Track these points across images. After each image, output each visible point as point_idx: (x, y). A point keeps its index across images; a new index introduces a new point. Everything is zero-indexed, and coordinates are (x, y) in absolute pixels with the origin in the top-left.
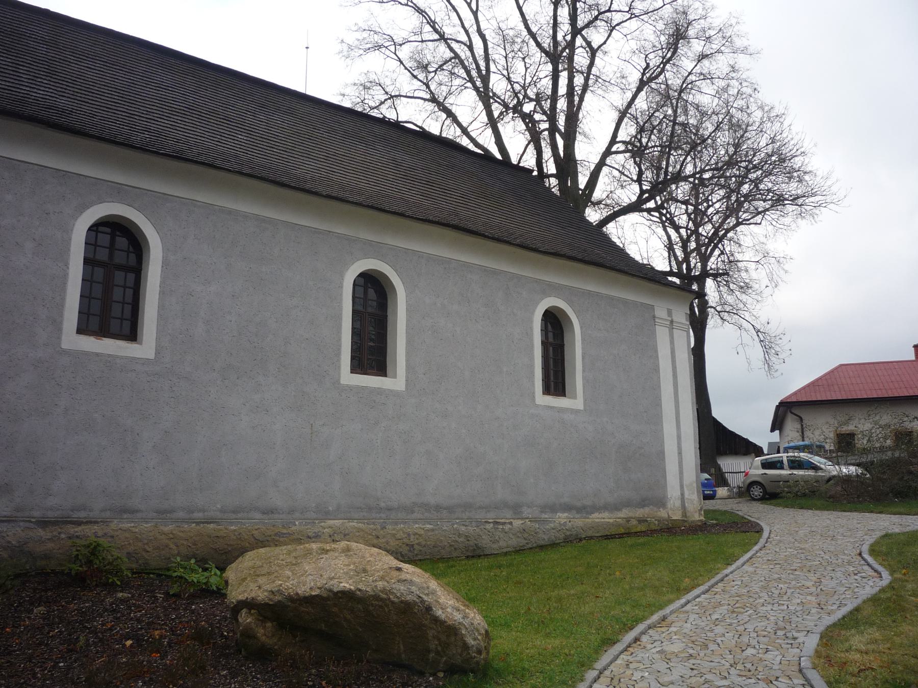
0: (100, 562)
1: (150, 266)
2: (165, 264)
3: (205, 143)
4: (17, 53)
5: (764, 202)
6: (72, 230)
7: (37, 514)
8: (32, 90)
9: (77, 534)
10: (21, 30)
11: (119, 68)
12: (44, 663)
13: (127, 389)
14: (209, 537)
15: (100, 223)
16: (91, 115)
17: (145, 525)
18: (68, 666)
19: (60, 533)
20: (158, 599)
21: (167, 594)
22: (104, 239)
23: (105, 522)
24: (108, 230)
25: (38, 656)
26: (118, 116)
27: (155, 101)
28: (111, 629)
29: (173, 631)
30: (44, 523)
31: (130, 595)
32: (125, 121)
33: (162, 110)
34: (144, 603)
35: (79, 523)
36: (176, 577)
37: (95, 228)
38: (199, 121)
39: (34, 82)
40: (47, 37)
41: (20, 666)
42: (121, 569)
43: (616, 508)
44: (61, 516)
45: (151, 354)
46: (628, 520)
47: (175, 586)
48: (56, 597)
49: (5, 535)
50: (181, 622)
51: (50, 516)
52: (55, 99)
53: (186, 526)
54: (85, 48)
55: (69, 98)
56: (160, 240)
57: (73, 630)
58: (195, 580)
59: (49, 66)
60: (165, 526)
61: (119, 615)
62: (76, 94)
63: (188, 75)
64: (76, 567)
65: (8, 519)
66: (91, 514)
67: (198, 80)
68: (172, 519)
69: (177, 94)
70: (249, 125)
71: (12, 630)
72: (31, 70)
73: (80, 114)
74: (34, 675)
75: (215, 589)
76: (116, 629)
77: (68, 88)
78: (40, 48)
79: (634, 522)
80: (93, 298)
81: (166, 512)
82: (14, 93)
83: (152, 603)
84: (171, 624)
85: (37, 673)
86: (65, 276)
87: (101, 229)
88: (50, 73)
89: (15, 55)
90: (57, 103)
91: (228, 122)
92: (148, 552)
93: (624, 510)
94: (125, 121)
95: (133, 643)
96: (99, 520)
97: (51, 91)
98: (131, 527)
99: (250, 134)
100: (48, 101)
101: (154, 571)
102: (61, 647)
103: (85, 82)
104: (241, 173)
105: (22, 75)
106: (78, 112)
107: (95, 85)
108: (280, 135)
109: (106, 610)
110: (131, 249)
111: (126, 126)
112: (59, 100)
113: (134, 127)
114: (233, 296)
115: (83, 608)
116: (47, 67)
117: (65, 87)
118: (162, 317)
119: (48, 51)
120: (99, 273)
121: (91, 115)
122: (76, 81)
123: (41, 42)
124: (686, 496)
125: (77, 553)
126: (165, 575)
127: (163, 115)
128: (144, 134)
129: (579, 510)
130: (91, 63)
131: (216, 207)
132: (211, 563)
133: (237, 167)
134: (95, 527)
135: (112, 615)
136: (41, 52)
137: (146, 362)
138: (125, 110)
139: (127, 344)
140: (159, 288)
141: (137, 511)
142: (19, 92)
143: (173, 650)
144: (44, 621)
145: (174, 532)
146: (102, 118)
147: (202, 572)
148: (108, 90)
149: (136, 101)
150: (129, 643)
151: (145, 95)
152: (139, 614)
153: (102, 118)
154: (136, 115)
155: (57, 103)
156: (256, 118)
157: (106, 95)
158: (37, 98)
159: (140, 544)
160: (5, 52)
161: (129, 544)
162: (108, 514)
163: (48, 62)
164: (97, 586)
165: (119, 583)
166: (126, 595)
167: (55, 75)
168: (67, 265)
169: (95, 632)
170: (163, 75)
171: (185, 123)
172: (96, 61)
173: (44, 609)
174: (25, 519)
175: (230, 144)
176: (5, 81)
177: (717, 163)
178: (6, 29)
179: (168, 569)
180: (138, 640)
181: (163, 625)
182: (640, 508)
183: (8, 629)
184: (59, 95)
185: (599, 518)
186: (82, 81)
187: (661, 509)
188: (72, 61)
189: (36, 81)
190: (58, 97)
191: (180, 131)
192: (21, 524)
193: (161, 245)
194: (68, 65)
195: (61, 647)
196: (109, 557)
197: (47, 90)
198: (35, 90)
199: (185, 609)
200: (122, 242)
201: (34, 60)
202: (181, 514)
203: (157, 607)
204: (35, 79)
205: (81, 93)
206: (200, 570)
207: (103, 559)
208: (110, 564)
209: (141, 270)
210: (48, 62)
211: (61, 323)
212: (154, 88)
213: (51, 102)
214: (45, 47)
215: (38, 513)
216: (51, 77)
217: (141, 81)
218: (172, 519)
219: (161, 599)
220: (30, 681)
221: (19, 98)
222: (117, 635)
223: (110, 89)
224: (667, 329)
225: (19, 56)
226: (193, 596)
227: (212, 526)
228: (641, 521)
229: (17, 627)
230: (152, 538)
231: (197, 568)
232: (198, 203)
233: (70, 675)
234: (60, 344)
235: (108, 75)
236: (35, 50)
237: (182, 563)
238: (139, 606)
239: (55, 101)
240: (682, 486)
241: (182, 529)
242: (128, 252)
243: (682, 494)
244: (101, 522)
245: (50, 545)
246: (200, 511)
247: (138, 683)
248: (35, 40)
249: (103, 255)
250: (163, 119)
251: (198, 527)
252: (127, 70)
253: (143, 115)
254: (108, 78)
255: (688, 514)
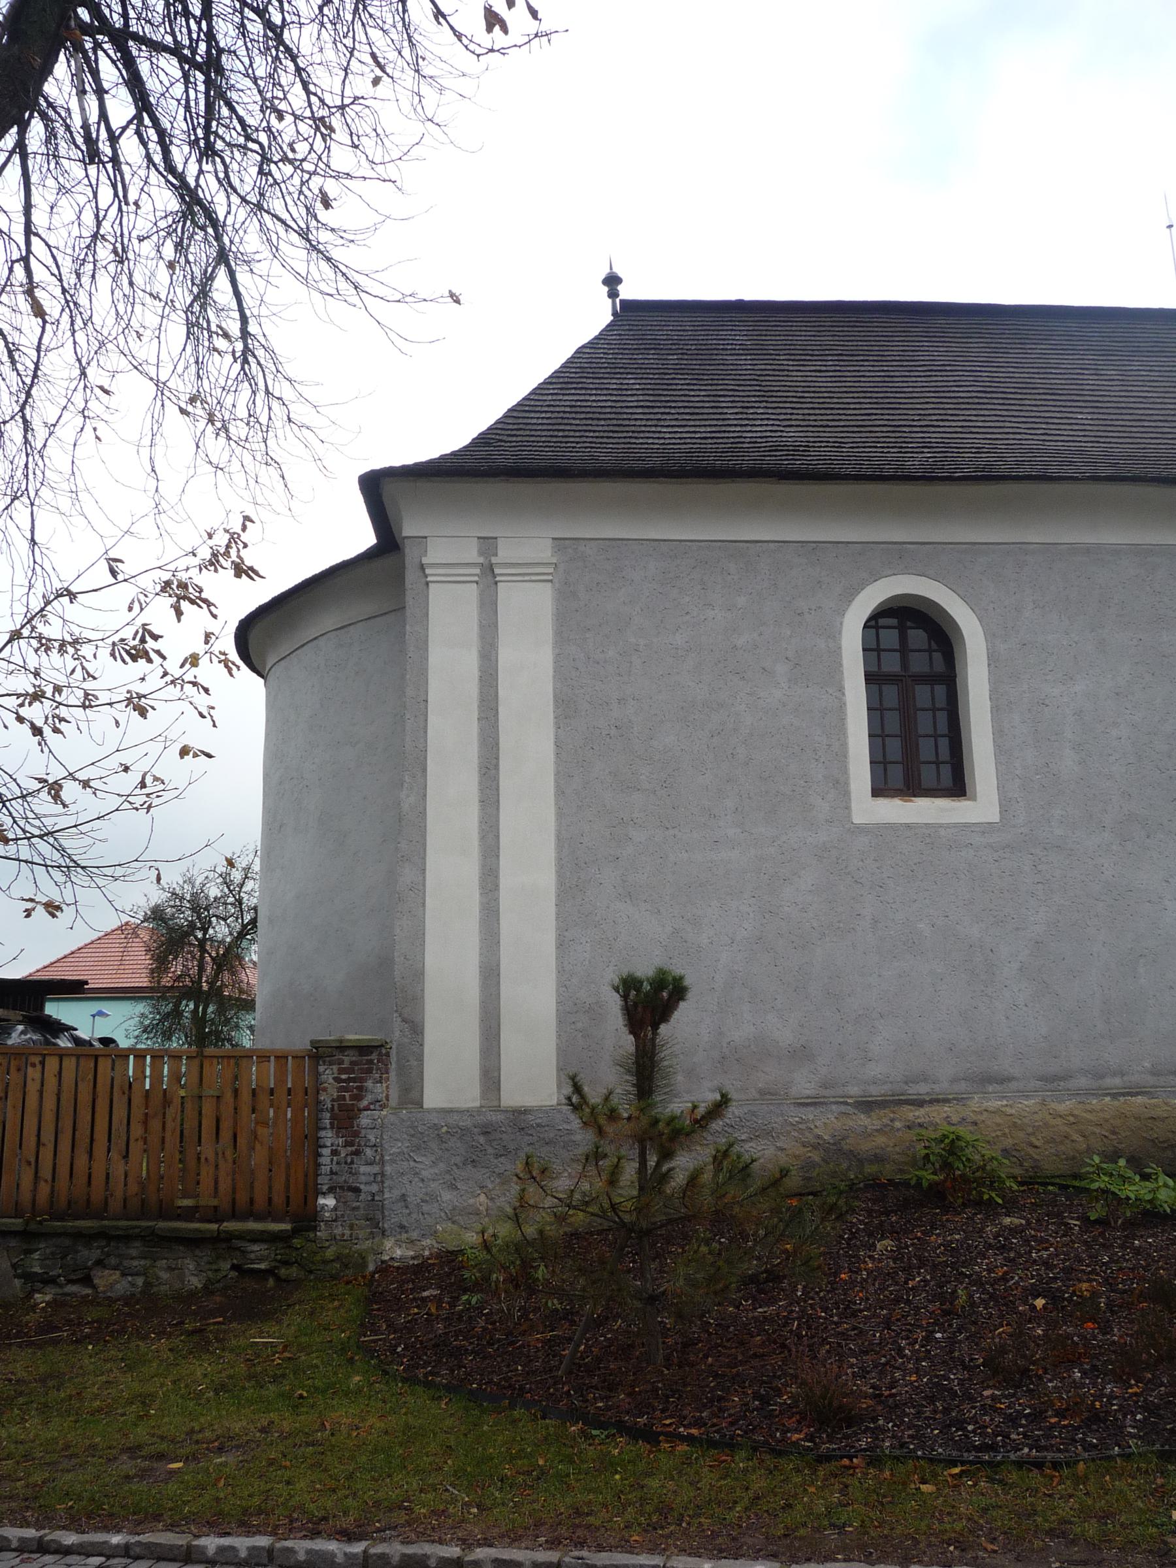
0: (964, 1165)
1: (969, 668)
2: (993, 659)
3: (1024, 442)
4: (712, 379)
6: (840, 633)
7: (854, 1090)
8: (744, 429)
9: (919, 1121)
10: (710, 342)
11: (862, 358)
12: (910, 1331)
13: (963, 876)
14: (1137, 1118)
15: (878, 613)
16: (836, 445)
17: (1026, 1103)
18: (949, 1338)
19: (892, 1120)
20: (1071, 1229)
21: (1085, 1219)
22: (890, 638)
23: (960, 1100)
24: (893, 622)
25: (898, 1320)
26: (877, 435)
27: (928, 395)
28: (1004, 1278)
29: (1111, 1284)
30: (867, 1105)
31: (1023, 1222)
32: (888, 440)
33: (942, 406)
34: (1051, 1236)
35: (920, 1103)
36: (1096, 1190)
37: (873, 623)
38: (1005, 407)
39: (745, 416)
40: (749, 343)
41: (875, 1336)
42: (1000, 1177)
44: (890, 1093)
45: (993, 815)
47: (1099, 1206)
48: (905, 1225)
49: (812, 1127)
50: (1120, 1269)
51: (874, 1094)
52: (780, 434)
53: (1094, 1102)
54: (805, 343)
55: (799, 426)
56: (978, 623)
57: (943, 1279)
58: (1132, 1196)
59: (760, 386)
60: (1059, 1102)
61: (1012, 1255)
62: (807, 417)
63: (971, 338)
64: (928, 1176)
65: (813, 1100)
66: (937, 1088)
67: (989, 340)
68: (1069, 1090)
69: (961, 373)
70: (1091, 393)
71: (850, 1277)
72: (737, 399)
73: (821, 447)
74: (900, 1351)
75: (1168, 1210)
76: (1013, 1278)
77: (795, 411)
78: (742, 362)
80: (887, 736)
81: (1055, 1078)
82: (721, 441)
83: (1064, 1236)
84: (1105, 1272)
85: (904, 1348)
86: (842, 707)
87: (882, 622)
88: (764, 396)
89: (710, 382)
90: (784, 439)
91: (1054, 397)
92: (1036, 1147)
94: (888, 440)
95: (1047, 1303)
96: (951, 1097)
97: (771, 422)
98: (1002, 1106)
99: (1097, 407)
100: (770, 439)
101: (1053, 1180)
102: (931, 1307)
103: (817, 395)
104: (1095, 479)
105: (725, 411)
106: (816, 445)
107: (832, 395)
108: (1150, 395)
109: (990, 1246)
110: (934, 646)
111: (892, 447)
112: (785, 434)
113: (904, 445)
114: (1117, 694)
115: (951, 1242)
116: (758, 388)
117: (789, 411)
118: (1001, 751)
119: (755, 362)
120: (891, 693)
121: (836, 445)
122: (803, 397)
123: (741, 352)
125: (927, 1151)
126: (1074, 1187)
127: (946, 414)
128: (923, 452)
130: (820, 363)
131: (1062, 546)
132: (1154, 1166)
133: (1088, 470)
134: (946, 1109)
135: (1002, 1254)
136: (744, 367)
137: (986, 828)
138: (886, 423)
139: (953, 803)
140: (989, 703)
141: (1010, 1079)
142: (728, 438)
143: (1119, 1317)
144: (895, 1263)
145: (1076, 1112)
146: (855, 445)
147: (1140, 1180)
148: (853, 398)
149: (900, 403)
150: (1040, 1303)
151: (911, 389)
152: (1045, 1254)
153: (855, 445)
154: (905, 426)
155: (784, 439)
156: (1102, 377)
157: (852, 406)
158: (754, 440)
159: (1021, 1135)
160: (695, 382)
161: (1004, 1135)
162: (963, 1086)
163: (757, 380)
164: (964, 1205)
165: (1000, 1201)
166: (1017, 1221)
167: (772, 396)
168: (841, 690)
169: (979, 1282)
170: (931, 349)
171: (983, 419)
172: (826, 358)
173: (891, 1243)
174: (838, 1099)
175: (1065, 433)
176: (705, 426)
177: (216, 134)
178: (689, 347)
179: (1076, 1176)
180: (1054, 1298)
181: (1090, 1273)
183: (843, 1276)
184: (784, 426)
186: (812, 395)
188: (791, 368)
189: (747, 413)
190: (782, 429)
191: (978, 433)
192: (834, 1107)
193: (981, 628)
194: (787, 376)
195: (931, 1307)
196: (977, 1157)
197: (766, 422)
198: (749, 428)
199: (1123, 1247)
200: (917, 637)
201: (738, 383)
202: (1083, 1082)
203: (1073, 1242)
204: (745, 410)
205: (815, 415)
206: (1137, 1178)
207: (968, 1160)
208: (983, 1168)
209: (956, 676)
210: (757, 380)
211: (847, 784)
212: (922, 374)
213: (775, 439)
214: (749, 357)
215: (856, 1089)
216: (767, 402)
217: (901, 369)
218: (1069, 1090)
219: (1077, 1228)
220: (896, 1360)
221: (730, 445)
222: (1017, 1288)
223: (856, 395)
225: (716, 382)
226: (1130, 1224)
227: (1140, 1099)
229: (856, 1273)
230: (1041, 1123)
231: (1130, 1173)
232: (1032, 547)
233: (957, 1354)
234: (849, 816)
235: (849, 374)
236: (735, 367)
237: (1104, 1166)
238: (1041, 1241)
239: (781, 436)
241: (1088, 1107)
242: (930, 651)
244: (954, 1099)
245: (881, 1140)
246: (1114, 1075)
247: (1074, 1373)
248: (733, 352)
249: (892, 664)
250: (948, 420)
251: (1116, 1103)
252: (875, 358)
253: (915, 423)
254: (849, 379)
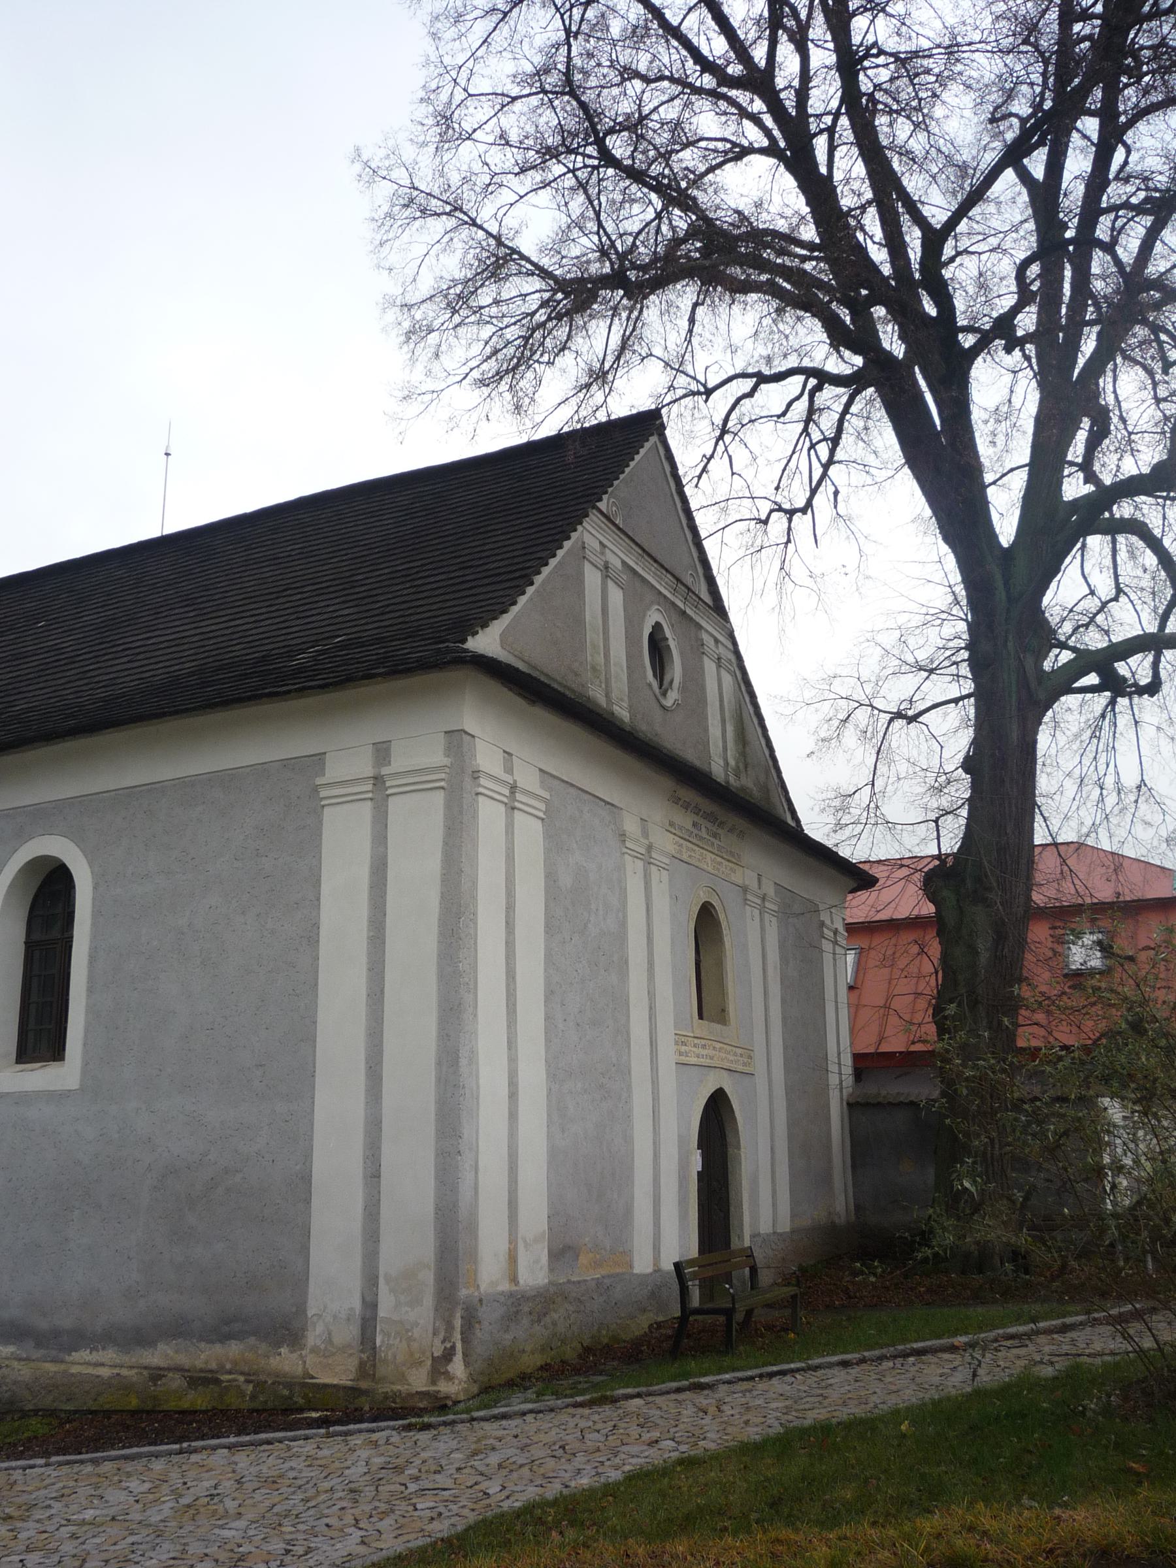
5: (1017, 231)
43: (140, 1338)
46: (157, 1374)
79: (176, 1382)
93: (161, 1346)
124: (385, 1309)
129: (41, 1339)
182: (212, 1342)
185: (88, 1364)
187: (284, 1350)
224: (502, 808)
228: (201, 1379)
240: (371, 1280)
243: (370, 1305)
255: (382, 1371)
